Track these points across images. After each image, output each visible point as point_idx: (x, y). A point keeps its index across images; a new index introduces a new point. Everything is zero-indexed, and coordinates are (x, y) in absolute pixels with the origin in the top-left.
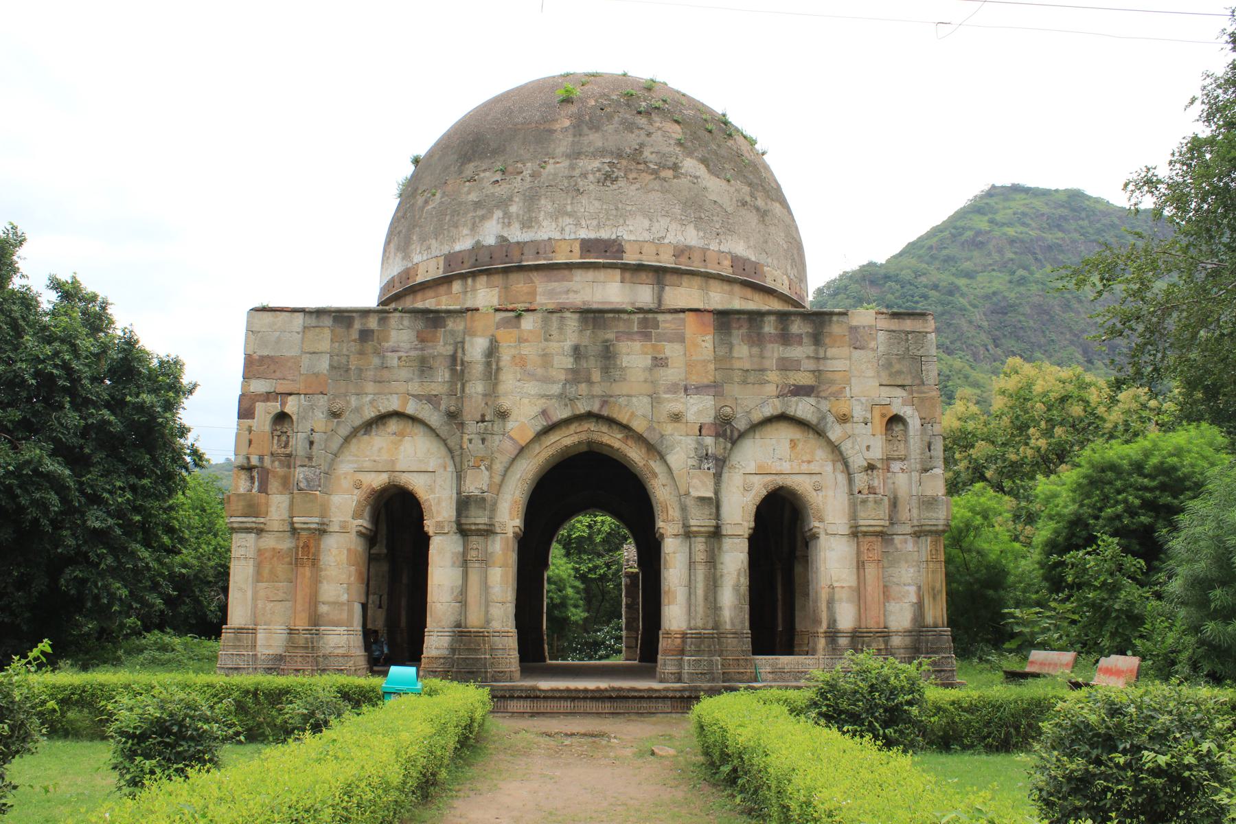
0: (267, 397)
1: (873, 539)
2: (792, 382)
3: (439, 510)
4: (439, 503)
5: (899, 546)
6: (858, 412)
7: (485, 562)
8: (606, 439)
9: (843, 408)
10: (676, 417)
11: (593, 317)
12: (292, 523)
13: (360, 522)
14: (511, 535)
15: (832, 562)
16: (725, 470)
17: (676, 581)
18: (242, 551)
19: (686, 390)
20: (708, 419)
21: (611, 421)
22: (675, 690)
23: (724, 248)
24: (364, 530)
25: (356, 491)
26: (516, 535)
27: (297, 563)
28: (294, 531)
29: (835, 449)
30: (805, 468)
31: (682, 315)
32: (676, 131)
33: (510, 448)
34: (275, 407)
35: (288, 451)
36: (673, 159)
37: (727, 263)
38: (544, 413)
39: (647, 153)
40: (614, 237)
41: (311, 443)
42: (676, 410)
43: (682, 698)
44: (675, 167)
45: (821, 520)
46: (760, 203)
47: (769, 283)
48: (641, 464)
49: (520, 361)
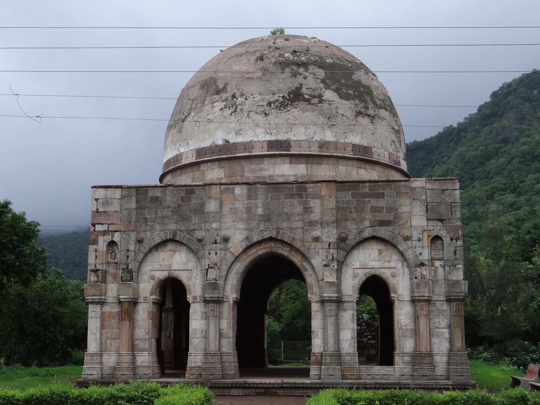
0: (104, 233)
1: (424, 303)
2: (379, 218)
3: (195, 287)
4: (194, 286)
5: (439, 307)
6: (416, 235)
7: (219, 317)
8: (280, 251)
9: (407, 233)
10: (317, 239)
11: (275, 186)
12: (119, 299)
13: (154, 297)
14: (231, 302)
15: (403, 315)
16: (344, 266)
17: (318, 326)
18: (94, 314)
19: (321, 224)
20: (333, 239)
21: (282, 242)
22: (316, 384)
23: (348, 141)
24: (156, 301)
25: (151, 281)
26: (235, 302)
27: (122, 319)
28: (120, 303)
29: (402, 254)
30: (387, 265)
31: (319, 184)
32: (321, 73)
33: (230, 258)
34: (108, 238)
35: (116, 261)
36: (319, 92)
37: (349, 149)
38: (247, 238)
39: (304, 90)
40: (285, 139)
41: (128, 257)
42: (316, 236)
43: (315, 388)
44: (320, 96)
45: (396, 293)
46: (371, 112)
47: (375, 158)
48: (299, 264)
49: (234, 211)
